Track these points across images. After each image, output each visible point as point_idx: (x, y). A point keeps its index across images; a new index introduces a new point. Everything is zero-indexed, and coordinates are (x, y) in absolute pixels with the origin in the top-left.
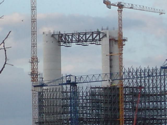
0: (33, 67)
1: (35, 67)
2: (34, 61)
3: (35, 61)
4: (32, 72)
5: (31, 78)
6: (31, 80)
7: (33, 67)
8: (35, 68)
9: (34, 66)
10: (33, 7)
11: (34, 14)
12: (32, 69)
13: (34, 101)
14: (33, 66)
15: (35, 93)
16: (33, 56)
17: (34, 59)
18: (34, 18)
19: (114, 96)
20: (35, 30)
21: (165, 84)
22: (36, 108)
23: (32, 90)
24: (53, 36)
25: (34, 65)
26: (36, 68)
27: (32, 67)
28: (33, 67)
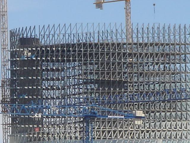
0: (4, 94)
1: (7, 94)
2: (5, 85)
3: (6, 84)
4: (2, 99)
5: (2, 108)
6: (1, 111)
7: (4, 94)
8: (6, 94)
9: (4, 92)
10: (4, 62)
11: (4, 38)
12: (2, 96)
13: (6, 139)
14: (4, 91)
15: (7, 128)
16: (4, 78)
17: (4, 82)
18: (4, 10)
19: (109, 132)
20: (7, 77)
21: (87, 26)
22: (8, 132)
23: (3, 124)
24: (25, 42)
25: (4, 90)
26: (8, 94)
27: (2, 94)
28: (3, 93)
